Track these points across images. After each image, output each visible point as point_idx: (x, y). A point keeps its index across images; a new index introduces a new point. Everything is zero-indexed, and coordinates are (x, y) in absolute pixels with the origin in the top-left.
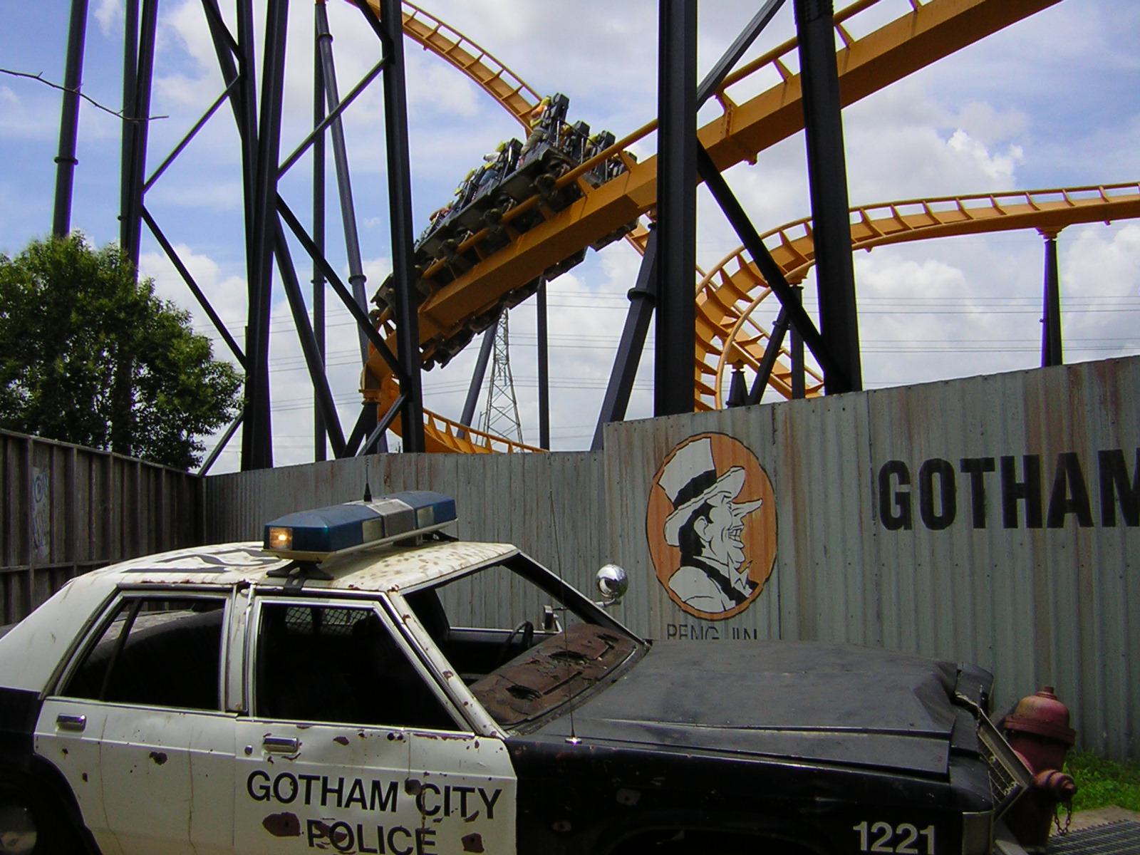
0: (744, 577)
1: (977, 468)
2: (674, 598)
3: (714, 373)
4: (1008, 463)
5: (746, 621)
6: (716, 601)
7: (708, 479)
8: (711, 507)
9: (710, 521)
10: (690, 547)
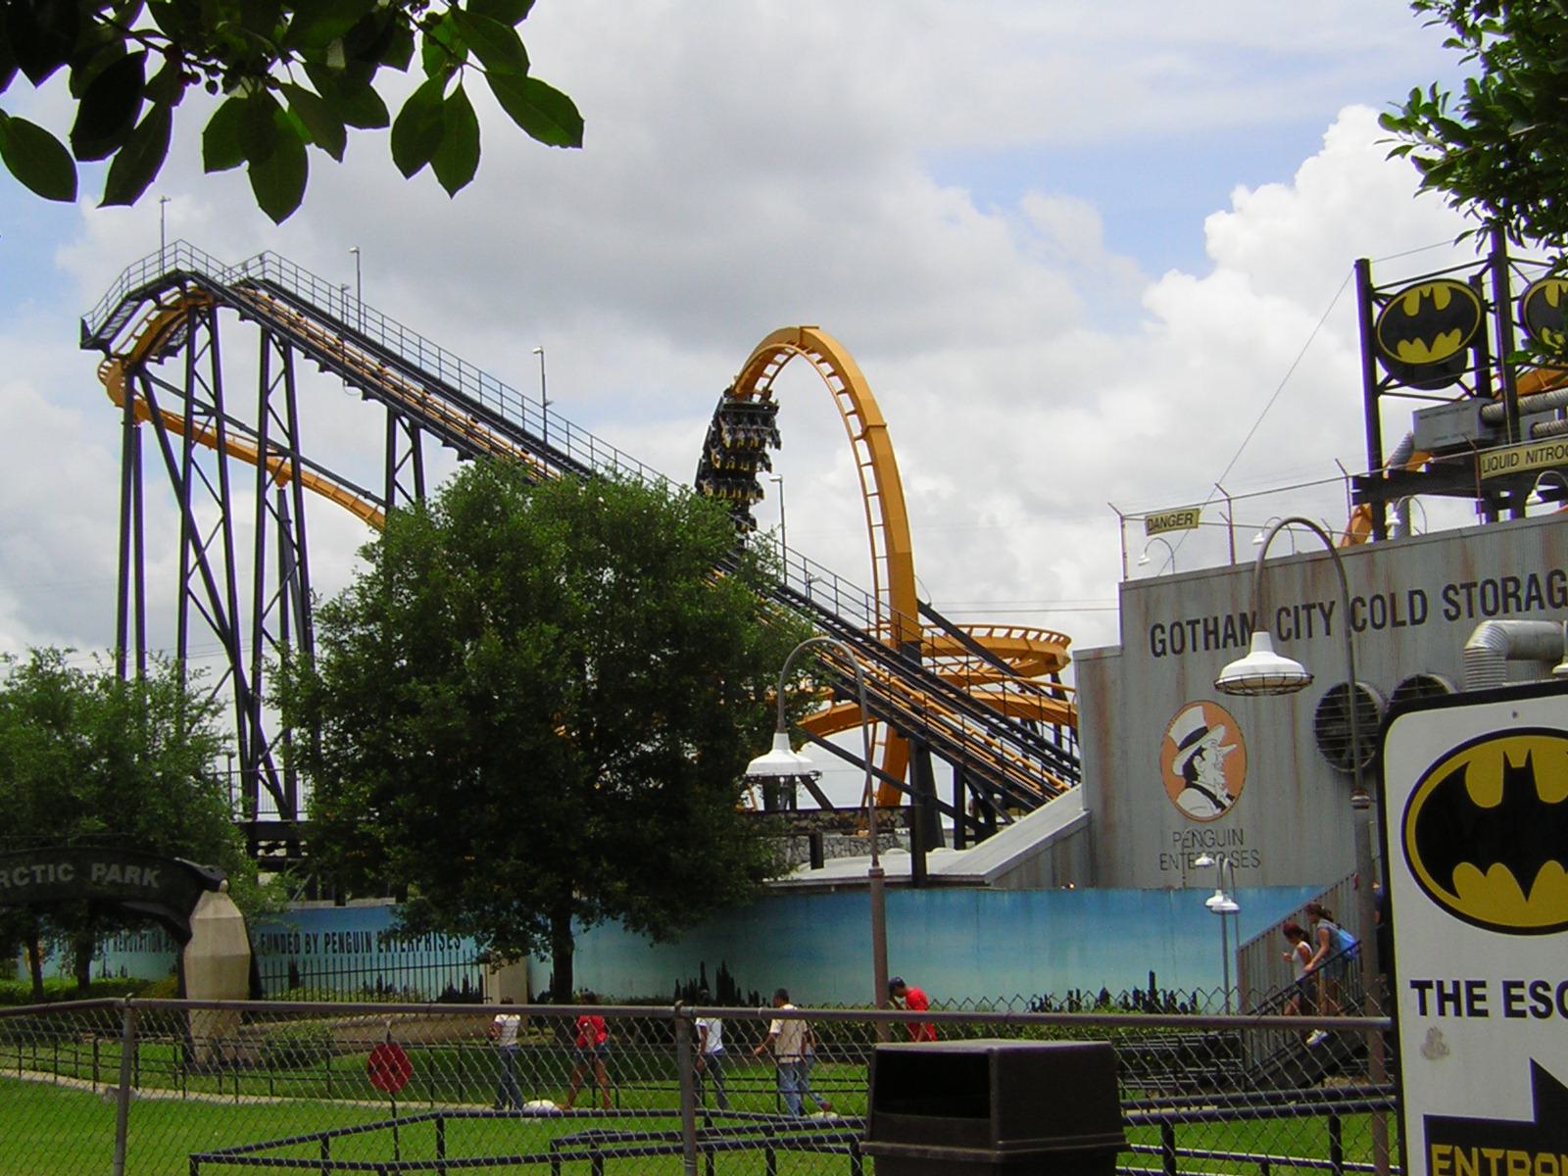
0: (1224, 793)
1: (1193, 623)
2: (1181, 810)
3: (828, 376)
4: (1206, 620)
5: (1229, 823)
6: (1209, 810)
7: (1203, 732)
8: (1203, 750)
9: (1204, 759)
10: (1190, 774)
